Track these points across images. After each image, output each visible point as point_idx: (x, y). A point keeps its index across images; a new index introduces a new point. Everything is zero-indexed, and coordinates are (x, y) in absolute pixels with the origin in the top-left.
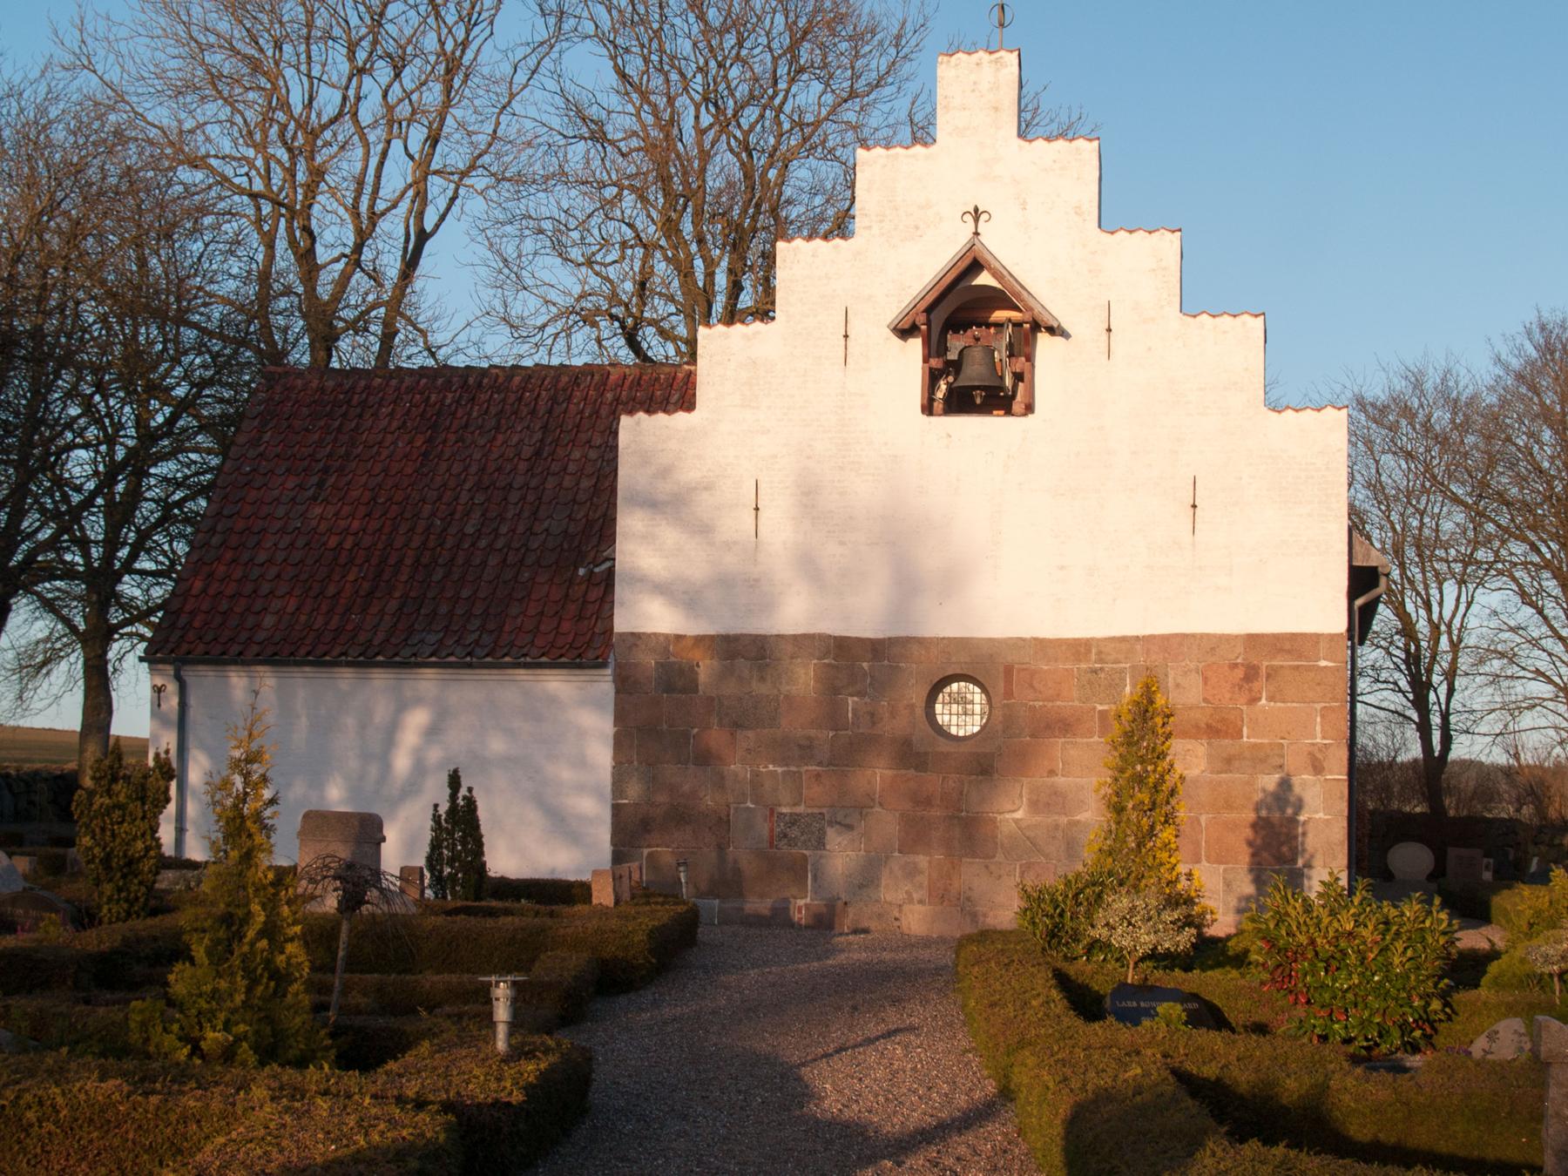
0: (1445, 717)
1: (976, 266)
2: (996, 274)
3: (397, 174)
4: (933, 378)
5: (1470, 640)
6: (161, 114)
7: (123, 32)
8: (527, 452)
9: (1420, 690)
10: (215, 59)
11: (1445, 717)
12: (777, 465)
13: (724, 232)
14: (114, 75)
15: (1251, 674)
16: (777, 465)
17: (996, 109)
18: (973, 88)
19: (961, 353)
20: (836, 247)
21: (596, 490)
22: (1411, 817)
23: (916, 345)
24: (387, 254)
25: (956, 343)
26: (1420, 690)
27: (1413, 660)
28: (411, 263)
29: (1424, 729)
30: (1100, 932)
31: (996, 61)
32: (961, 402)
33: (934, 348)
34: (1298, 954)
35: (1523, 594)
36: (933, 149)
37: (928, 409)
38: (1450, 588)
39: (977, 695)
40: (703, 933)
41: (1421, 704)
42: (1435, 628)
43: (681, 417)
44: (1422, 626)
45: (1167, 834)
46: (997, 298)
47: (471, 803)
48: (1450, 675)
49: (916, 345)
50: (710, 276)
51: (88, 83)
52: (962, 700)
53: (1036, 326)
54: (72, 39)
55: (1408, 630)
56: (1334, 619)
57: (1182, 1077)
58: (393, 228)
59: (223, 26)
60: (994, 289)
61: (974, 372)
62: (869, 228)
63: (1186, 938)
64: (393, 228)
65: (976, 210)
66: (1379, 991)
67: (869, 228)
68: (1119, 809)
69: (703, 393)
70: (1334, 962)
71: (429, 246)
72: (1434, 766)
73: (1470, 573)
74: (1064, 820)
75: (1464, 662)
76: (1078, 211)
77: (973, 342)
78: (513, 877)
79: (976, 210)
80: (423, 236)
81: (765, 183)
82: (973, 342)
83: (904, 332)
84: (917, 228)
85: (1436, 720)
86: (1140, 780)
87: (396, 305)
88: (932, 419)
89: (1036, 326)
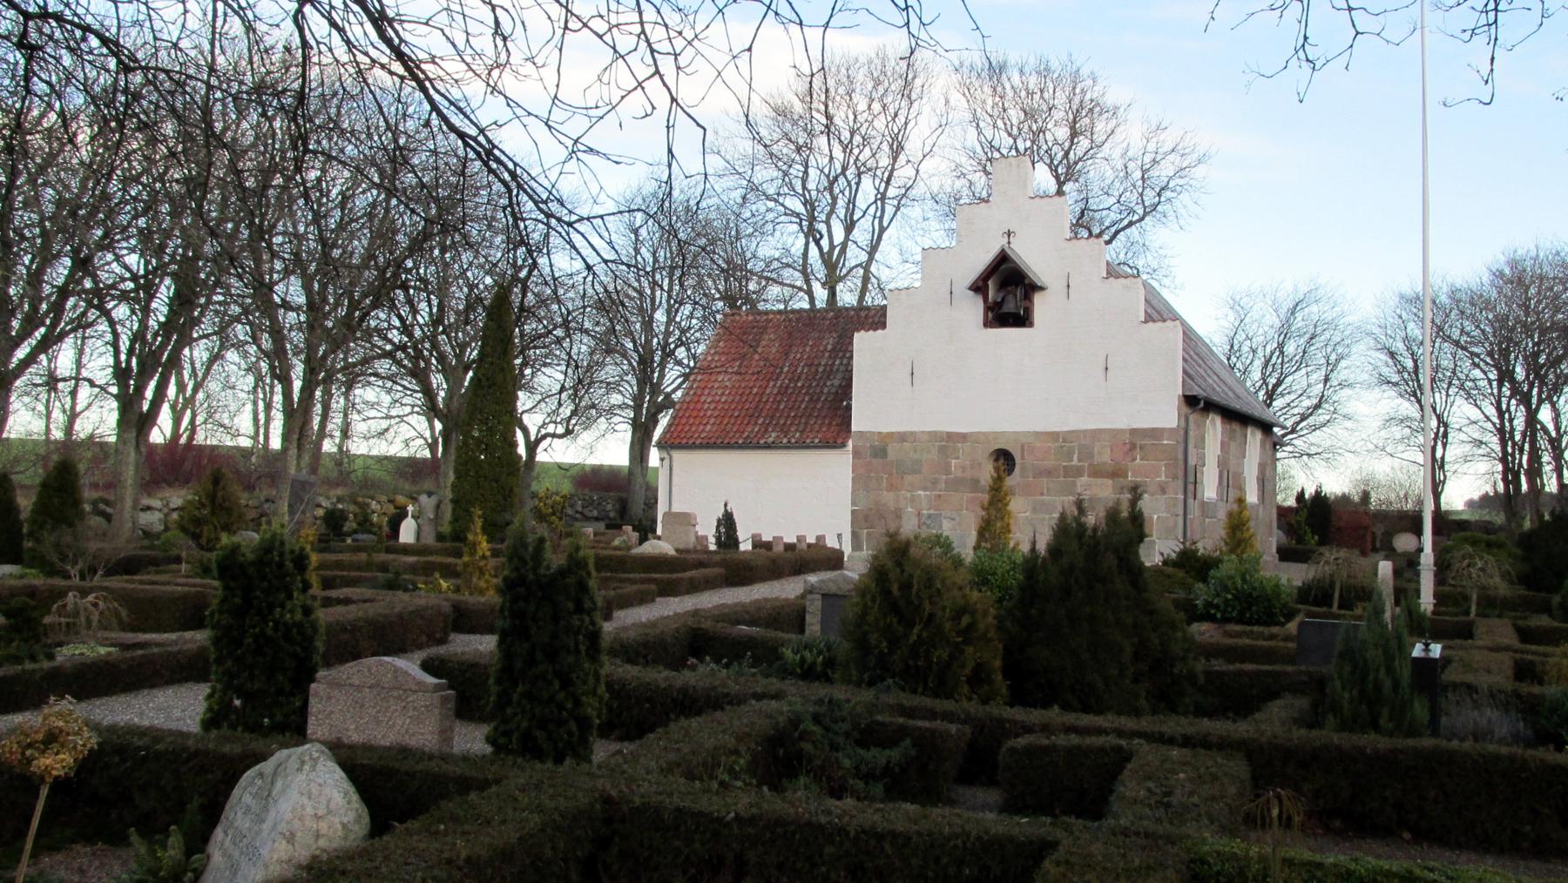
15: (1133, 447)
80: (882, 230)
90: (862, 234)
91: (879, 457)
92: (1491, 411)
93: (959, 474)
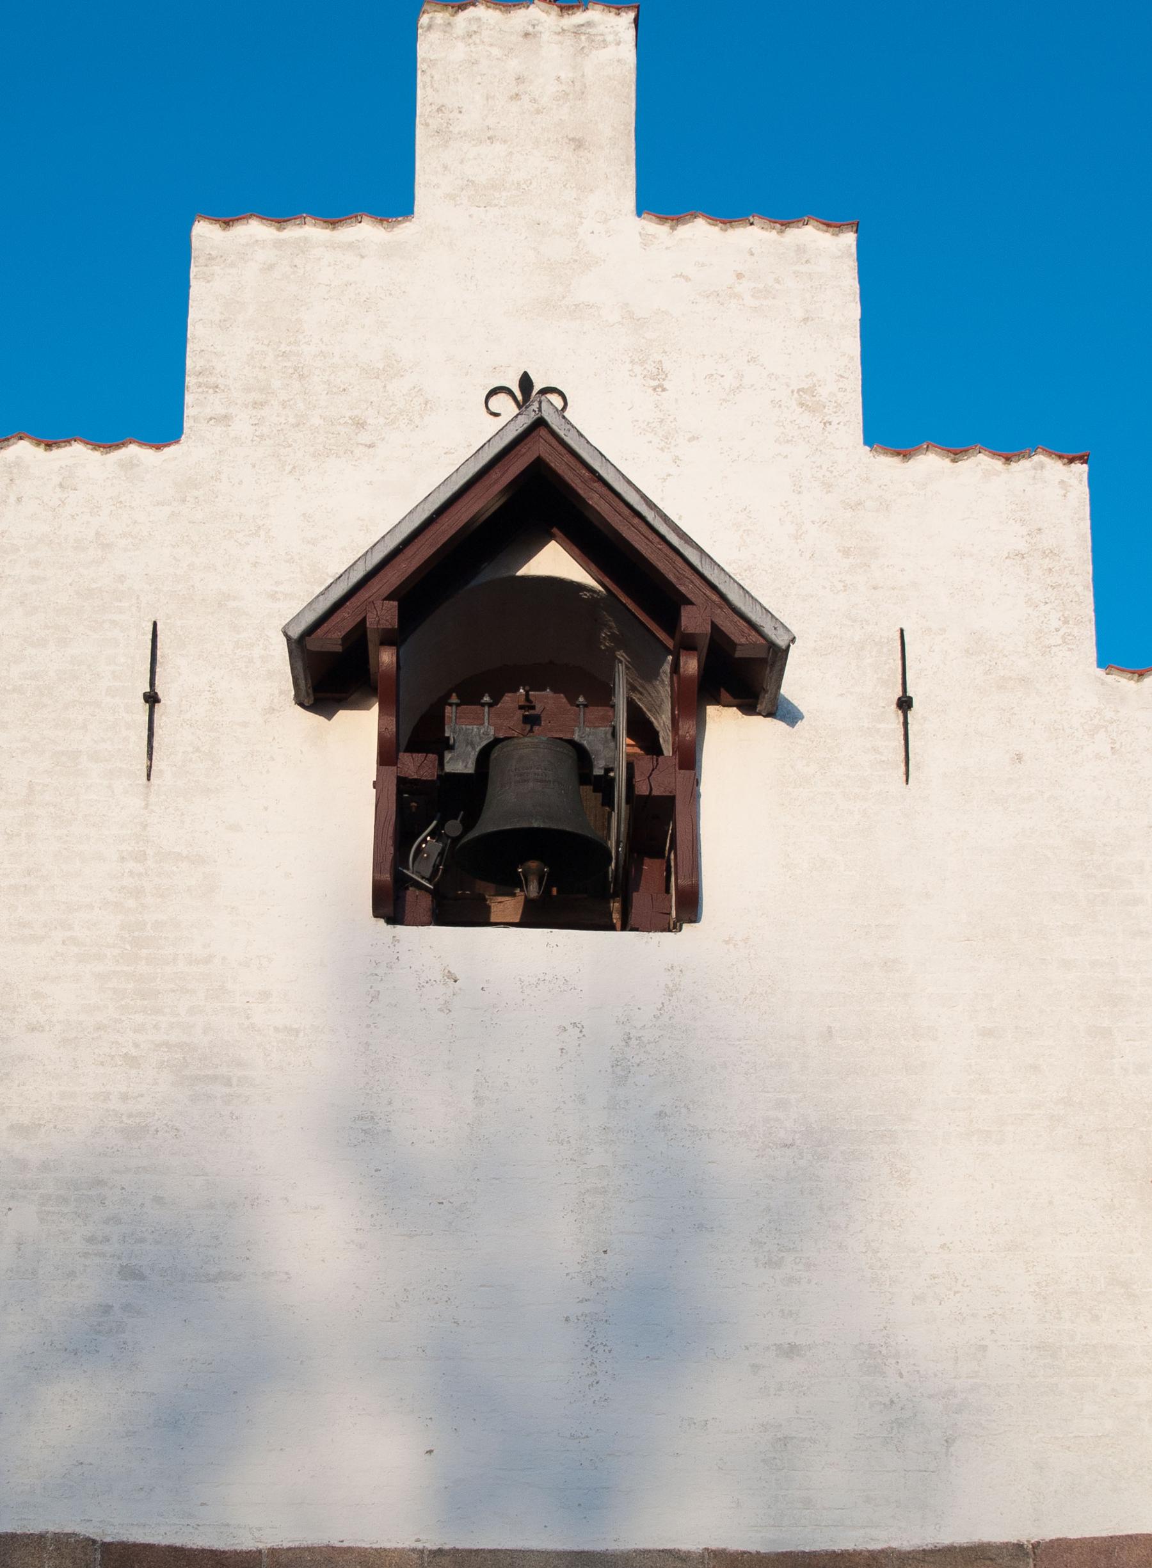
2: (595, 540)
17: (578, 144)
18: (522, 107)
19: (484, 757)
20: (129, 466)
23: (360, 729)
25: (469, 733)
31: (577, 31)
36: (405, 231)
49: (360, 729)
60: (580, 587)
61: (526, 796)
62: (225, 419)
65: (526, 382)
67: (225, 419)
76: (808, 398)
78: (763, 1550)
79: (526, 382)
83: (329, 670)
84: (360, 425)
88: (401, 930)
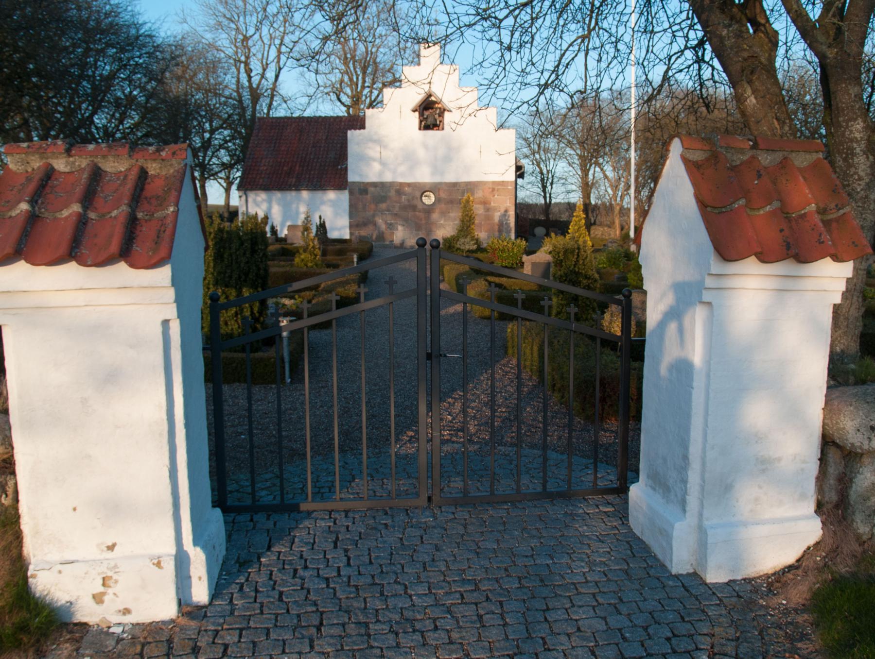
0: (550, 194)
1: (430, 96)
3: (273, 53)
4: (421, 122)
5: (557, 175)
6: (209, 36)
7: (195, 13)
8: (324, 138)
9: (544, 187)
10: (221, 19)
11: (550, 194)
12: (390, 146)
13: (369, 78)
14: (193, 24)
15: (493, 190)
16: (390, 146)
21: (341, 147)
22: (541, 220)
24: (270, 74)
25: (426, 113)
26: (544, 187)
27: (542, 180)
28: (277, 77)
29: (545, 197)
30: (458, 246)
32: (427, 127)
33: (421, 115)
34: (496, 250)
35: (569, 164)
37: (420, 129)
38: (552, 161)
39: (432, 195)
40: (375, 250)
41: (544, 191)
42: (548, 171)
43: (362, 131)
44: (545, 172)
45: (473, 226)
46: (435, 103)
47: (324, 222)
48: (552, 184)
49: (417, 114)
50: (357, 78)
51: (186, 27)
52: (428, 196)
53: (444, 110)
54: (181, 15)
55: (542, 173)
56: (511, 176)
57: (472, 269)
58: (272, 68)
59: (222, 10)
61: (430, 121)
63: (475, 247)
64: (272, 68)
66: (511, 256)
68: (463, 221)
69: (368, 123)
70: (503, 251)
71: (282, 71)
72: (548, 206)
73: (558, 156)
74: (633, 90)
75: (555, 180)
77: (430, 113)
80: (280, 69)
81: (372, 53)
82: (430, 113)
83: (414, 111)
85: (548, 195)
86: (467, 215)
87: (273, 89)
89: (444, 110)
90: (270, 74)
91: (367, 199)
92: (578, 168)
93: (406, 203)
